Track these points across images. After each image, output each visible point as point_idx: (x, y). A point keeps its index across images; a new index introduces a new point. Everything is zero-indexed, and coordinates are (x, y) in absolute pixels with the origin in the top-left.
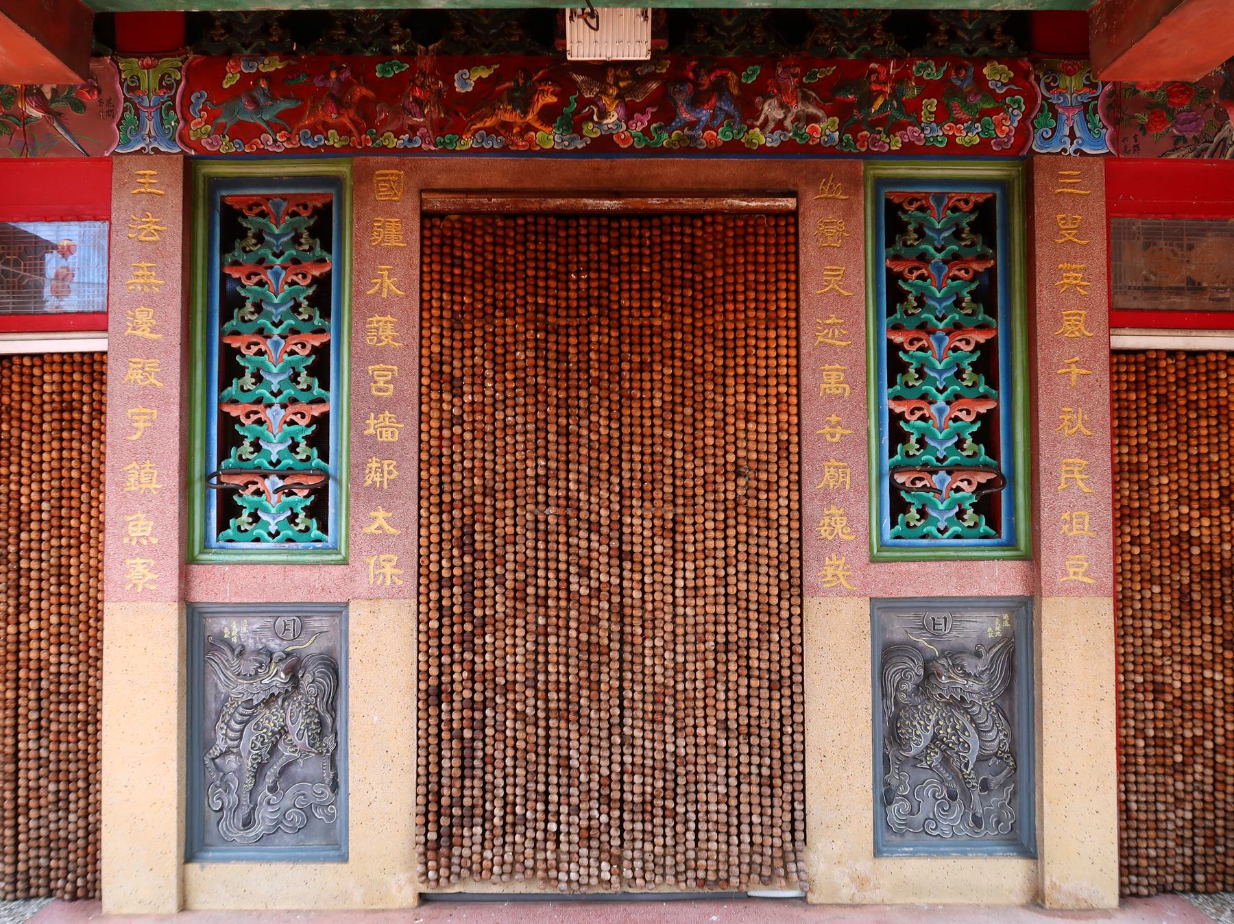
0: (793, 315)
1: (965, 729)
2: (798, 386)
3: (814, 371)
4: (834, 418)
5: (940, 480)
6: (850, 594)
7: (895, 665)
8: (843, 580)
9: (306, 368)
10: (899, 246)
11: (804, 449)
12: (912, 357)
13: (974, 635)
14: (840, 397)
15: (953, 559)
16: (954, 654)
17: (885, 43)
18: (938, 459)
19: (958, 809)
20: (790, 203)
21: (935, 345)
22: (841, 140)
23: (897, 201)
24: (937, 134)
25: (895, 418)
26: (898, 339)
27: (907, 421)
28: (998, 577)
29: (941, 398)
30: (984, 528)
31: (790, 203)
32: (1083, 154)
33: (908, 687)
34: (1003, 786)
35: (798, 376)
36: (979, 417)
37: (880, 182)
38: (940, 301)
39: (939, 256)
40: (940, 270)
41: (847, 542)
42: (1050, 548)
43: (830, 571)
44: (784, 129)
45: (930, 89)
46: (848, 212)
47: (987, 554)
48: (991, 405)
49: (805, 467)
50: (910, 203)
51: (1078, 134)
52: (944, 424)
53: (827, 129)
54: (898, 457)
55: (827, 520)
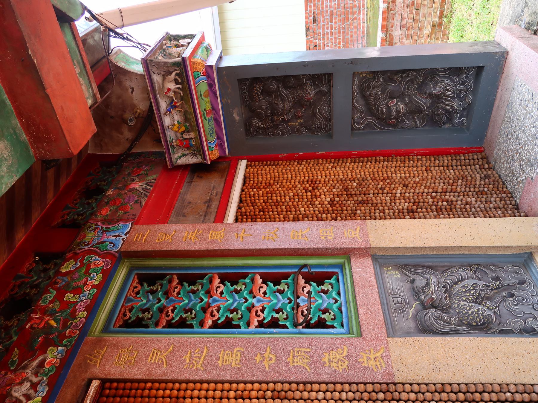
0: (177, 385)
1: (464, 287)
2: (231, 382)
3: (222, 370)
4: (258, 358)
5: (302, 301)
6: (387, 350)
7: (432, 324)
8: (378, 355)
9: (274, 286)
10: (150, 322)
11: (280, 379)
12: (222, 315)
13: (401, 284)
14: (243, 354)
15: (354, 291)
16: (416, 293)
17: (19, 320)
18: (290, 302)
19: (517, 293)
20: (95, 384)
21: (217, 303)
22: (65, 346)
23: (121, 323)
24: (88, 292)
25: (261, 325)
26: (210, 322)
27: (264, 319)
28: (362, 270)
29: (251, 300)
30: (333, 281)
31: (95, 384)
32: (128, 232)
33: (446, 317)
34: (492, 271)
35: (223, 383)
36: (264, 282)
37: (106, 329)
38: (190, 300)
39: (163, 301)
40: (172, 301)
41: (349, 351)
42: (342, 243)
43: (372, 363)
44: (38, 383)
45: (60, 296)
46: (117, 346)
47: (348, 276)
48: (258, 277)
49: (293, 378)
50: (125, 315)
51: (117, 234)
52: (268, 300)
53: (53, 355)
54: (288, 324)
55: (334, 364)
